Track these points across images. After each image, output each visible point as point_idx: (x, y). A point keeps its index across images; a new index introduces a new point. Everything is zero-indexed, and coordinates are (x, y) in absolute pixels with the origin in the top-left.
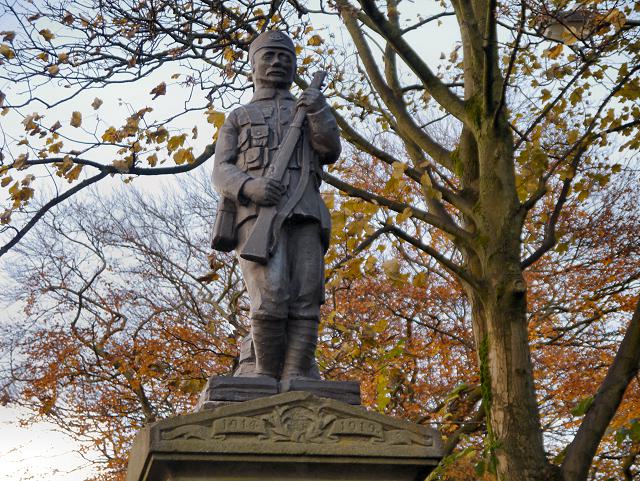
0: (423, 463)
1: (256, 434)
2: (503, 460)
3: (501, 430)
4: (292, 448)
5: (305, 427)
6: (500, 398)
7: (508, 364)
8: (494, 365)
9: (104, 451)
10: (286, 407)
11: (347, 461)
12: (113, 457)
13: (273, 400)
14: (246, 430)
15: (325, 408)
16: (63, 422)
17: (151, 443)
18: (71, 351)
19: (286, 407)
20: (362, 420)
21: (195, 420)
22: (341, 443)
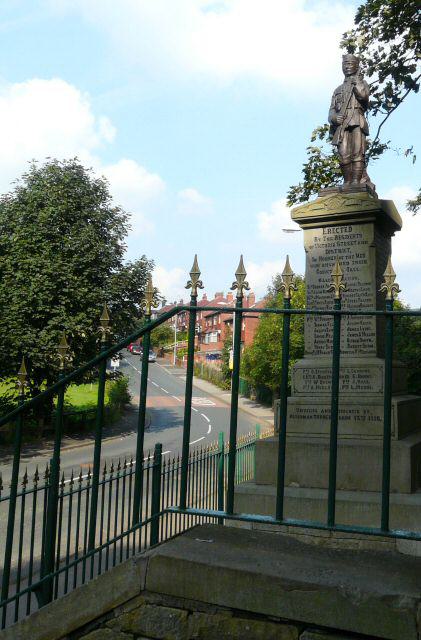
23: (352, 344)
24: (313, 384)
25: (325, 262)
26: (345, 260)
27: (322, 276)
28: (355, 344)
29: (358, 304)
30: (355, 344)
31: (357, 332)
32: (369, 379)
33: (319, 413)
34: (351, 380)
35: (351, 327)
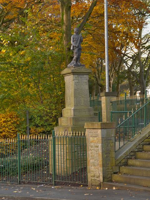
6: (65, 24)
7: (67, 18)
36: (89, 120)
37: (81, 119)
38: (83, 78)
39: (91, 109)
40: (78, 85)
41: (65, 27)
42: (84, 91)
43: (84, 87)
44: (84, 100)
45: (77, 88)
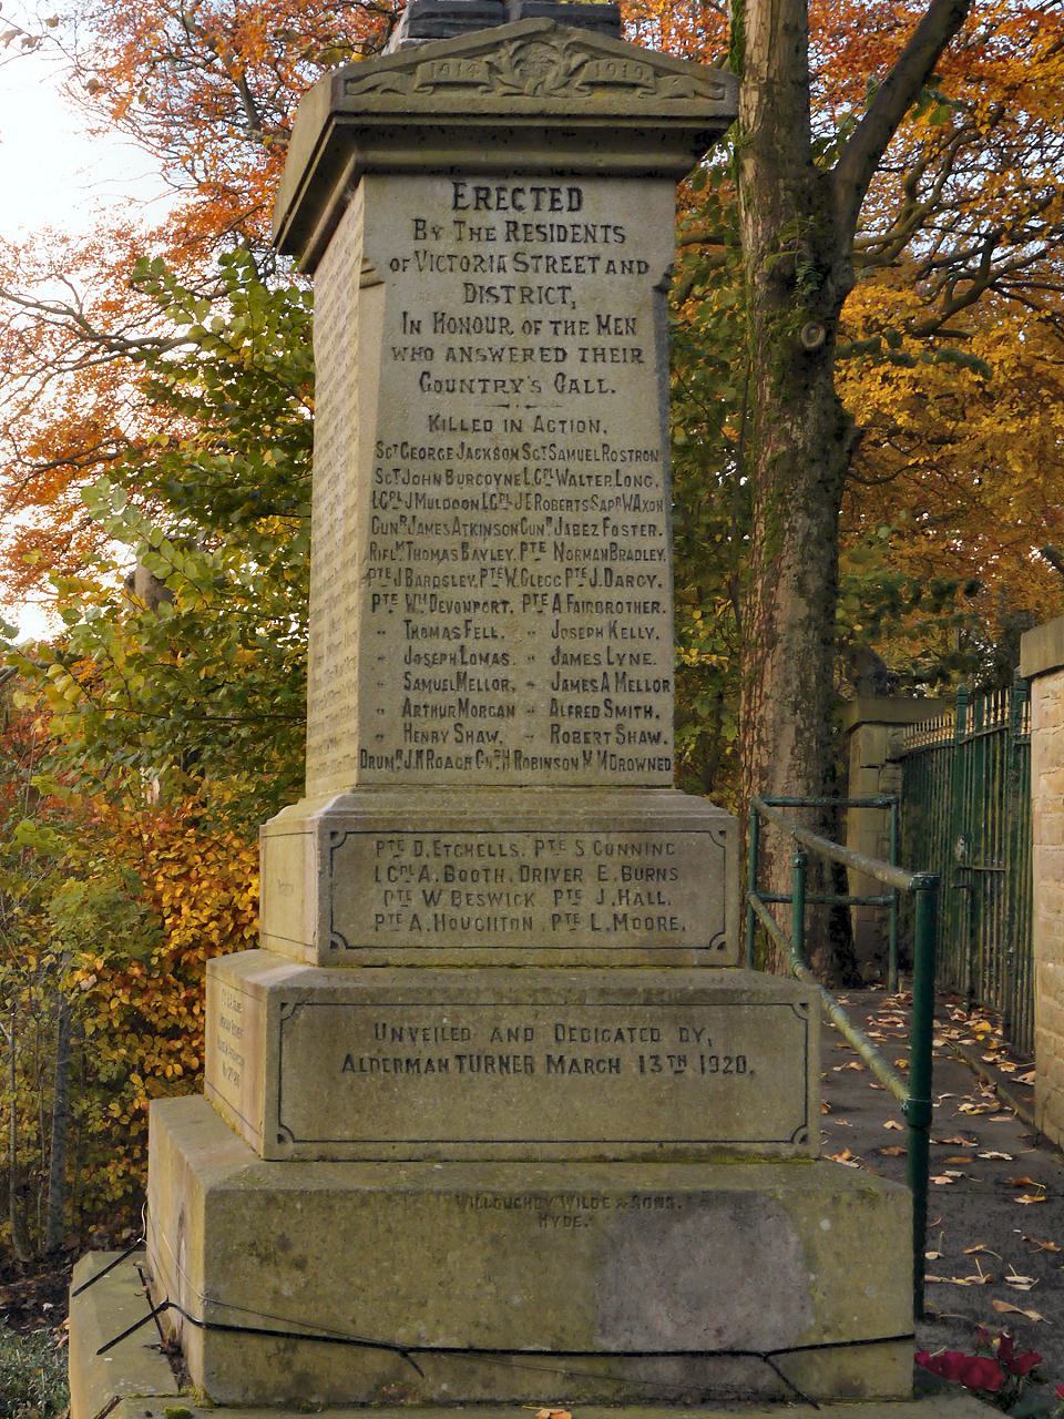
0: (709, 125)
1: (476, 85)
2: (749, 164)
3: (752, 120)
4: (526, 104)
5: (544, 72)
6: (755, 70)
7: (774, 17)
8: (753, 19)
9: (192, 172)
10: (517, 44)
11: (601, 124)
12: (204, 180)
13: (502, 31)
14: (463, 77)
15: (574, 43)
16: (140, 132)
17: (332, 99)
18: (152, 26)
19: (517, 44)
20: (625, 61)
21: (392, 64)
22: (593, 97)
23: (569, 724)
24: (416, 902)
25: (458, 340)
26: (545, 337)
27: (447, 406)
28: (582, 724)
29: (602, 542)
30: (582, 724)
31: (595, 673)
32: (665, 887)
33: (481, 1043)
34: (589, 888)
35: (570, 646)
36: (615, 1065)
37: (444, 1035)
38: (563, 234)
39: (689, 827)
40: (463, 370)
41: (755, 96)
42: (567, 479)
43: (577, 407)
44: (558, 657)
45: (433, 422)
